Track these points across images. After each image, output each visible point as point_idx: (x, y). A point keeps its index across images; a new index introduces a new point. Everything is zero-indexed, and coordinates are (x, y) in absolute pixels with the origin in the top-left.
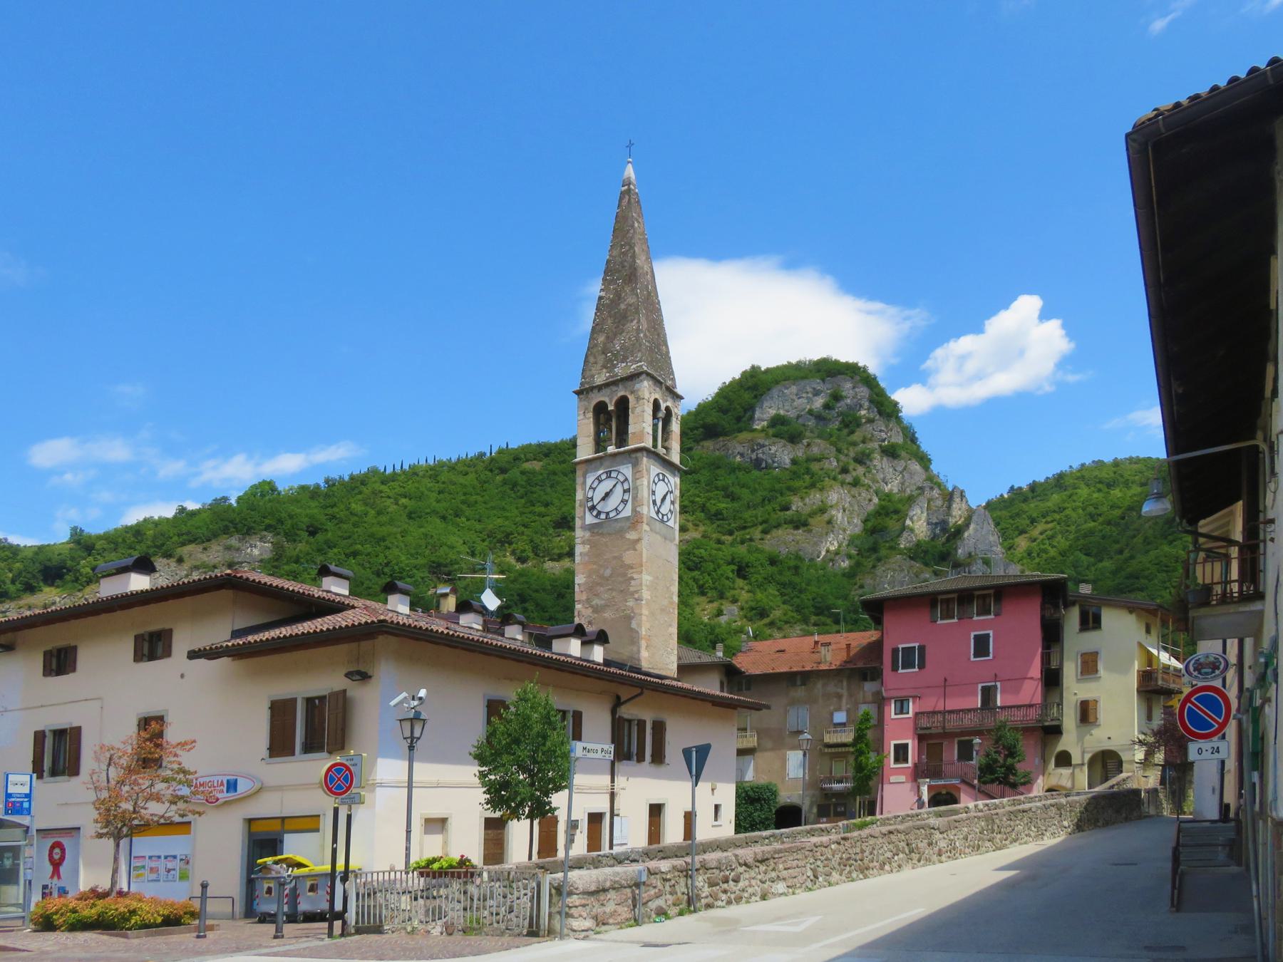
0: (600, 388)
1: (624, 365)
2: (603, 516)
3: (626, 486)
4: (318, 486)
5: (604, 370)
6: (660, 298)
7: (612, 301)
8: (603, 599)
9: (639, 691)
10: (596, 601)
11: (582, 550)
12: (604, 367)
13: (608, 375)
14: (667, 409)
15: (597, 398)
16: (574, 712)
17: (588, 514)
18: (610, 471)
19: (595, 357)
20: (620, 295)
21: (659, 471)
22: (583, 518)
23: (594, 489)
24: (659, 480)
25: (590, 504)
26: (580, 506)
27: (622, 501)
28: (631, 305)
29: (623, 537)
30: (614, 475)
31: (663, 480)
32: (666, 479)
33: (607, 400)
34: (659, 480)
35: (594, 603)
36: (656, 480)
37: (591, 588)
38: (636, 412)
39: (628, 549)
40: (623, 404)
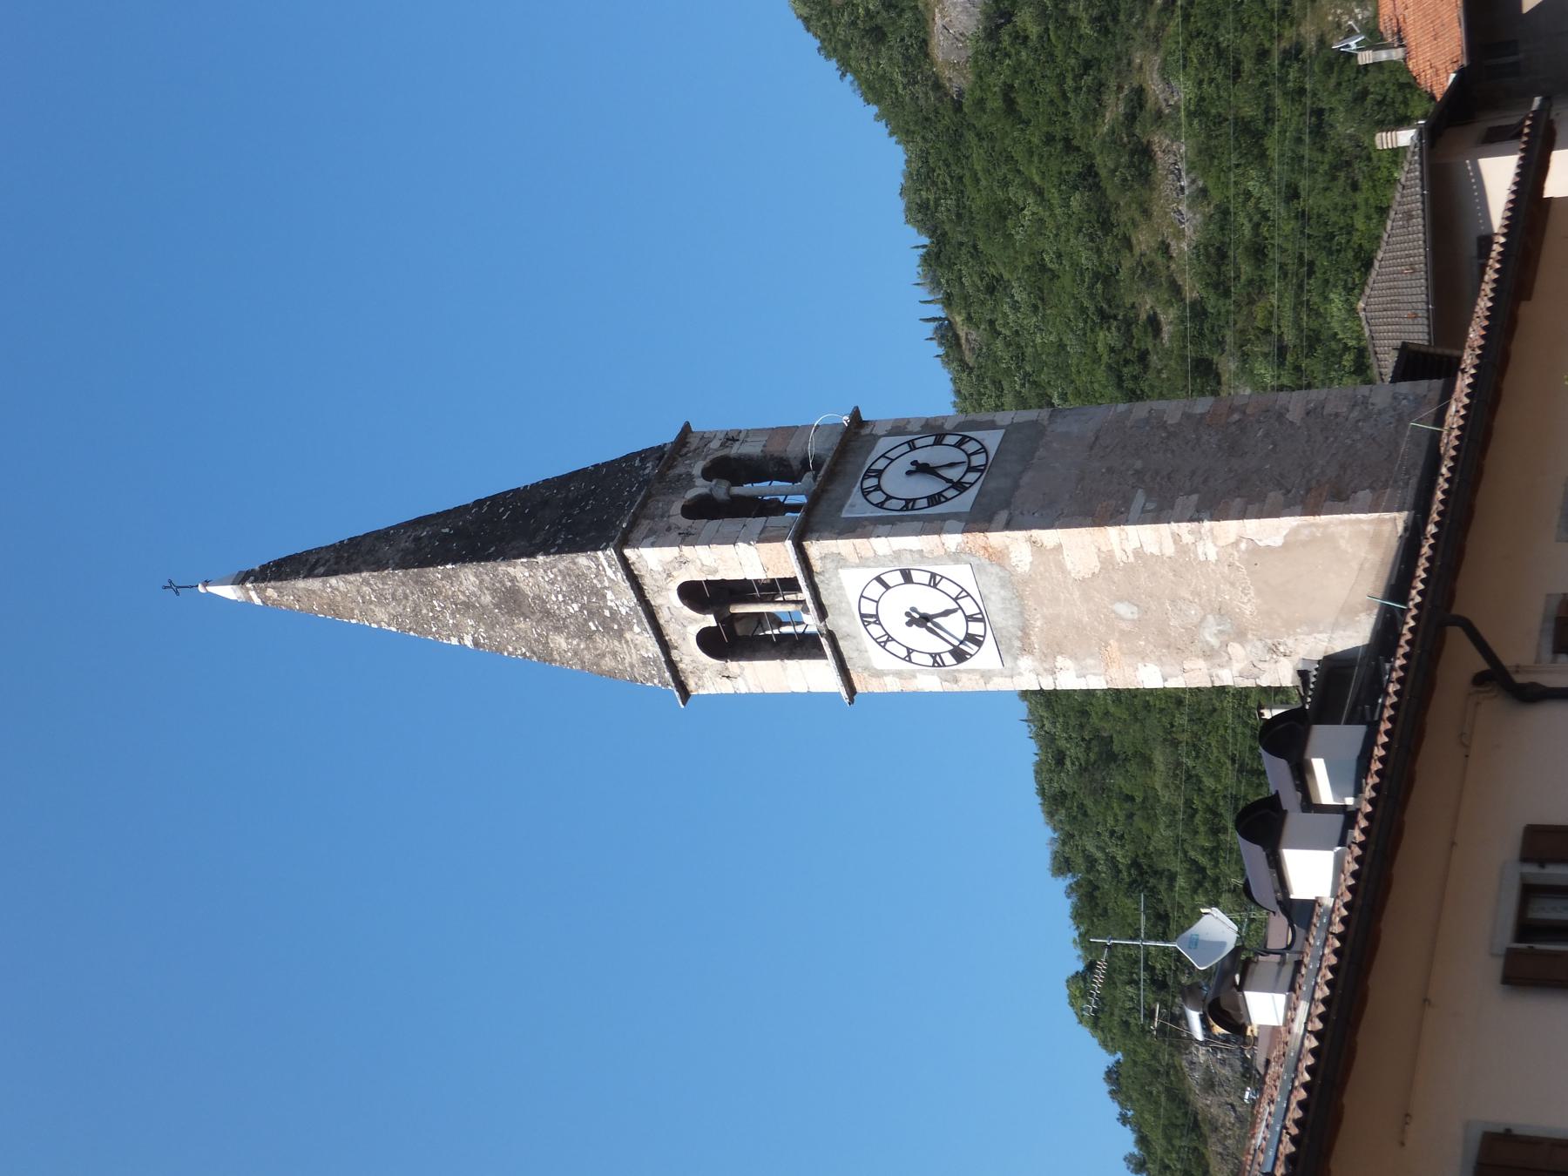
0: (665, 646)
1: (609, 595)
3: (894, 578)
4: (1071, 890)
5: (628, 636)
6: (469, 500)
7: (479, 620)
8: (1203, 619)
9: (1456, 635)
10: (1210, 635)
11: (1072, 674)
12: (620, 635)
13: (637, 629)
14: (707, 474)
15: (690, 655)
16: (1525, 858)
18: (862, 616)
19: (603, 655)
20: (463, 603)
21: (856, 496)
22: (986, 675)
23: (910, 651)
24: (878, 488)
25: (949, 659)
26: (956, 681)
27: (935, 586)
28: (482, 582)
29: (1026, 580)
30: (868, 608)
31: (879, 473)
32: (880, 465)
33: (693, 631)
34: (878, 488)
35: (1215, 642)
36: (877, 497)
37: (1175, 647)
38: (714, 565)
39: (1061, 567)
40: (694, 594)
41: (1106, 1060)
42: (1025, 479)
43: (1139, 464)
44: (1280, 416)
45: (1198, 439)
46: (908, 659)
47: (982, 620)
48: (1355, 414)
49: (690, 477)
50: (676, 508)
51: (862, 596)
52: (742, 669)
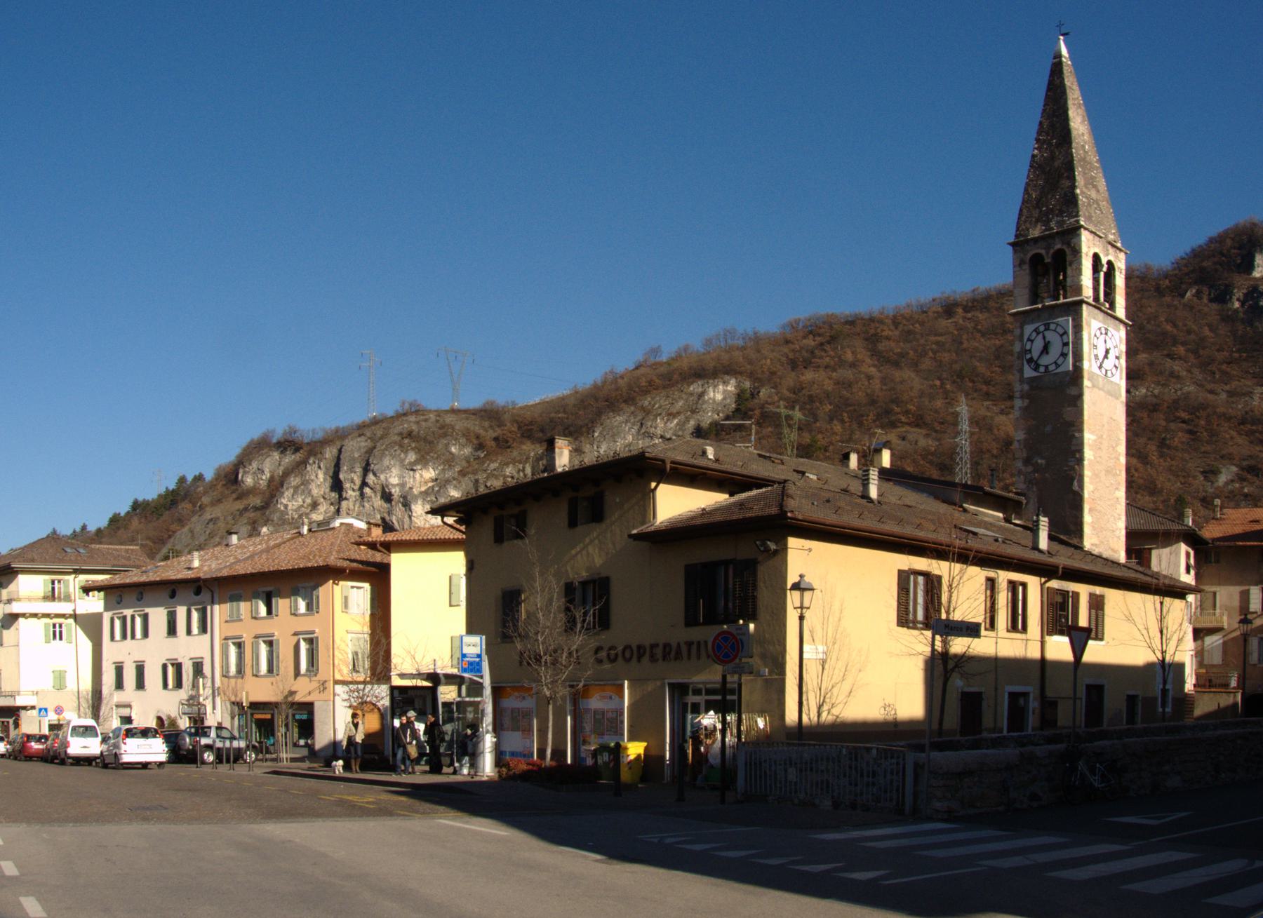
2: (1042, 369)
17: (1026, 367)
18: (1049, 324)
25: (1028, 356)
30: (1052, 327)
41: (122, 514)
42: (1101, 392)
43: (1104, 436)
44: (1117, 489)
45: (1111, 459)
46: (1029, 339)
47: (1046, 372)
48: (1117, 516)
49: (1107, 255)
50: (1097, 250)
51: (1058, 325)
52: (1024, 270)
